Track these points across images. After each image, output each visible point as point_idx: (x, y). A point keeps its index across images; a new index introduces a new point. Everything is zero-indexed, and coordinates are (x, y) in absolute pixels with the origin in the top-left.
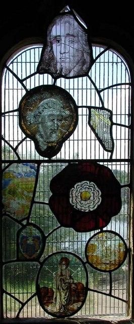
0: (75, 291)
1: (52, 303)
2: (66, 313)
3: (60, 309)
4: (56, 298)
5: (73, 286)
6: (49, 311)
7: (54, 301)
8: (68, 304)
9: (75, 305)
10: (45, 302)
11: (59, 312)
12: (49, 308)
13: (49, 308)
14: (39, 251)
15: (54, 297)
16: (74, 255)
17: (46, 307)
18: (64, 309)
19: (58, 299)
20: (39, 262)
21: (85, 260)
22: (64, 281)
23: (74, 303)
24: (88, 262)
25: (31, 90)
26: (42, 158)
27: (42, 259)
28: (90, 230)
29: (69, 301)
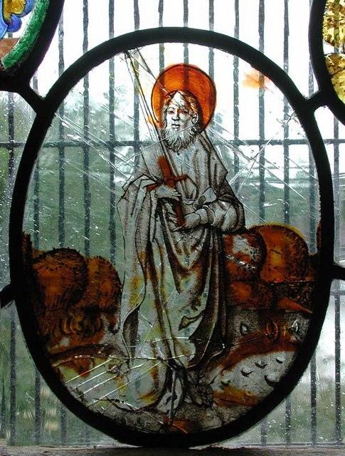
0: (252, 278)
1: (109, 350)
2: (195, 424)
3: (157, 393)
4: (133, 319)
5: (241, 245)
6: (104, 408)
7: (119, 340)
8: (202, 364)
9: (246, 365)
10: (65, 342)
11: (152, 409)
12: (96, 385)
13: (96, 385)
14: (27, 21)
15: (124, 314)
16: (243, 211)
17: (72, 380)
18: (186, 390)
19: (146, 326)
20: (31, 97)
21: (305, 83)
22: (181, 215)
23: (244, 354)
24: (326, 96)
25: (191, 362)
26: (172, 212)
27: (45, 79)
28: (306, 367)
29: (216, 346)
